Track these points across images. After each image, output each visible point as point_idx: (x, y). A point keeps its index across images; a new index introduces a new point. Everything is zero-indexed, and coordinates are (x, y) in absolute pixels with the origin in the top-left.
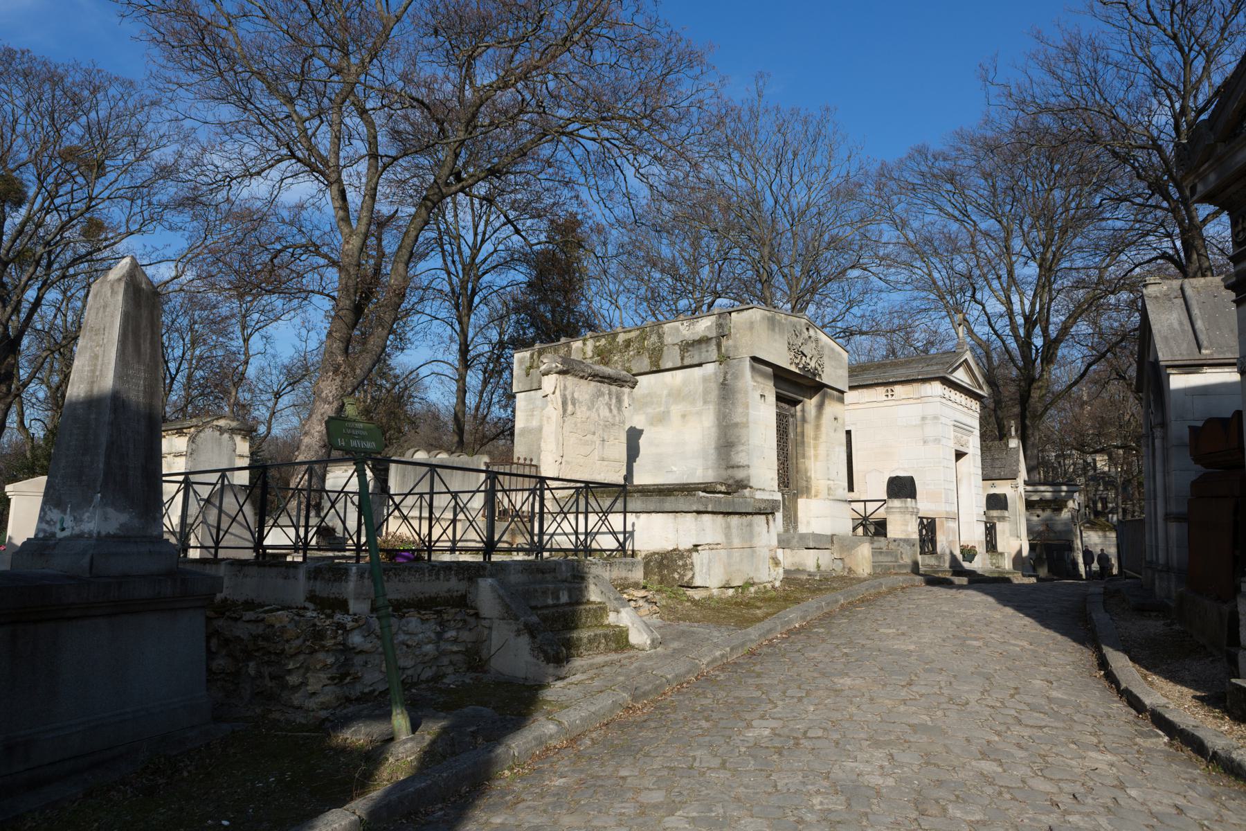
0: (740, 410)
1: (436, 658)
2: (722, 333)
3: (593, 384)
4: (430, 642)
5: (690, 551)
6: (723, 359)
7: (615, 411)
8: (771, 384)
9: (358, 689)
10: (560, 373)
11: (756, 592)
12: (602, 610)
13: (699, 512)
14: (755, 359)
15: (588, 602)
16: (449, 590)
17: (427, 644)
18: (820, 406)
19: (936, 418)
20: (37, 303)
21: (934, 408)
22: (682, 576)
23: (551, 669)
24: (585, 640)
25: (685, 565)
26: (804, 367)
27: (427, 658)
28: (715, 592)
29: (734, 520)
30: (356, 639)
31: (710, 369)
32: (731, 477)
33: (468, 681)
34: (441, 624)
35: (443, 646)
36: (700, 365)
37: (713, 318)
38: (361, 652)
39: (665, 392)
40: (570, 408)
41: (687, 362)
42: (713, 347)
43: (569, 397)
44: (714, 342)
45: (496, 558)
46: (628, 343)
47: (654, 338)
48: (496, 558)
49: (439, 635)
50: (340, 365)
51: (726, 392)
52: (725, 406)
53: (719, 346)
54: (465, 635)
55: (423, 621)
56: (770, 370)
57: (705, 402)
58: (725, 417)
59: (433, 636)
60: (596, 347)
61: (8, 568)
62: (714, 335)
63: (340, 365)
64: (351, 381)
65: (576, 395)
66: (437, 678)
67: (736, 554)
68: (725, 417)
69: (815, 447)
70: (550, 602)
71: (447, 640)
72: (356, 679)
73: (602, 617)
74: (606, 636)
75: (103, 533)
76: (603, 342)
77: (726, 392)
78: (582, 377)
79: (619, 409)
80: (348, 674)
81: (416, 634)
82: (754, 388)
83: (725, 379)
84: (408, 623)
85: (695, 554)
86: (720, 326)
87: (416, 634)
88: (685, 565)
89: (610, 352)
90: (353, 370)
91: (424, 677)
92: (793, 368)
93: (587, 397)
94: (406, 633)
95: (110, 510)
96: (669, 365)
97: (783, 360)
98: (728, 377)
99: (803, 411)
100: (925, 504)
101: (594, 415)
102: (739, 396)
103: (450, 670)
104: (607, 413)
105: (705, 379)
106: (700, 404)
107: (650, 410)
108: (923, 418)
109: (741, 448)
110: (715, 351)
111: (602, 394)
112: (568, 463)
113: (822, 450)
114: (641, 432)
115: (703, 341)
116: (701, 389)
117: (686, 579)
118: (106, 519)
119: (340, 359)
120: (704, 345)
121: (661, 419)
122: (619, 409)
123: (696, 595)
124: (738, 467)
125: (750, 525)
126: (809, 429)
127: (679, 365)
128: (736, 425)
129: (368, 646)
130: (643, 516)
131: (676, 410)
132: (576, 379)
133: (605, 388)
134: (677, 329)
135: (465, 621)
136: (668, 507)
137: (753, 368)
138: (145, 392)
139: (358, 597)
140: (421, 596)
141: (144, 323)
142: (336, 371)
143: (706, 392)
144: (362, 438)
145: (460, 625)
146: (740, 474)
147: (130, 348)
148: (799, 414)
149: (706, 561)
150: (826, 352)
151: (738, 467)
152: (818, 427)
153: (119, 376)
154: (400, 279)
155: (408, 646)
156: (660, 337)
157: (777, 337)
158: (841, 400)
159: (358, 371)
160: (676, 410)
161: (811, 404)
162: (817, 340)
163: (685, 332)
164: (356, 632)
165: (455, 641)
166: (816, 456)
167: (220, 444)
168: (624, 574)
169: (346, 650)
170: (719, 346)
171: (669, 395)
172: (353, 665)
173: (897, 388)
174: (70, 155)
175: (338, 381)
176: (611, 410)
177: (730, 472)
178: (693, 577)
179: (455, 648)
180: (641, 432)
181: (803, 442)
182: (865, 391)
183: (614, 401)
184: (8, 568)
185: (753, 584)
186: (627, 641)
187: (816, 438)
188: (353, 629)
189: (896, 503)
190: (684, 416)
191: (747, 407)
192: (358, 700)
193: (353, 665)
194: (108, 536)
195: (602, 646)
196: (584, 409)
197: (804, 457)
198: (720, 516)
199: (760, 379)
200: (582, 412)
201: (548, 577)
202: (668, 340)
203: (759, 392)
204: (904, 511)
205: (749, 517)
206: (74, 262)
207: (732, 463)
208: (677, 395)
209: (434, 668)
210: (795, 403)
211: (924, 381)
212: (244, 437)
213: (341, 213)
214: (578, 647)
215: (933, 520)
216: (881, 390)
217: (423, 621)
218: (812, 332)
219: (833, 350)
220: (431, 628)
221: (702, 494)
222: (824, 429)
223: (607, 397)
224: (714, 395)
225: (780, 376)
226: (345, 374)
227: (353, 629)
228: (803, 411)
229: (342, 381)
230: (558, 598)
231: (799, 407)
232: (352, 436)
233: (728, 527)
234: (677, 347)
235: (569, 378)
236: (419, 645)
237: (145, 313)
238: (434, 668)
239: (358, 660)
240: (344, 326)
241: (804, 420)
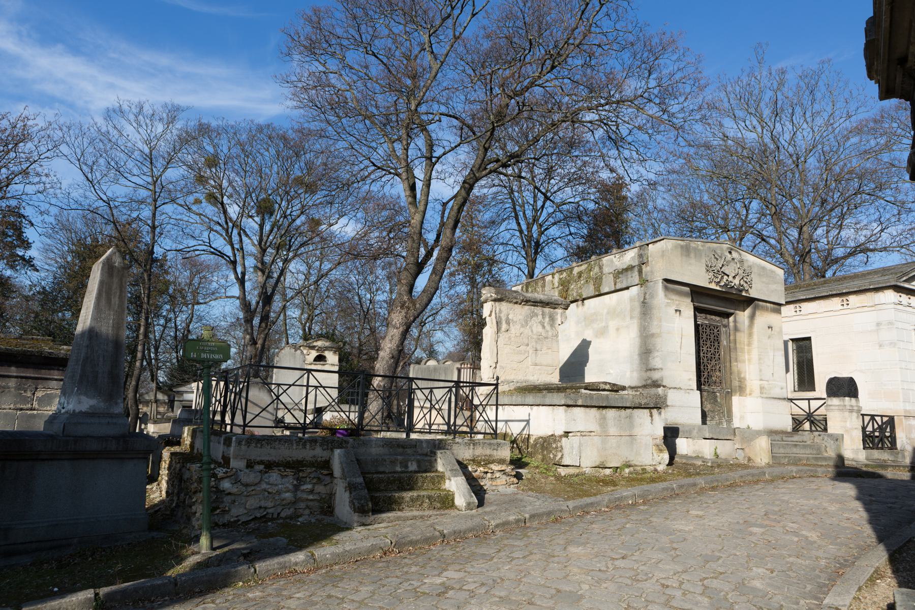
0: (655, 323)
1: (294, 503)
2: (643, 262)
3: (527, 307)
4: (288, 492)
5: (561, 437)
6: (643, 282)
7: (548, 327)
8: (689, 300)
9: (227, 518)
10: (495, 300)
11: (630, 473)
12: (442, 477)
13: (568, 406)
14: (667, 281)
15: (437, 471)
16: (314, 456)
17: (286, 492)
18: (752, 317)
19: (890, 323)
20: (282, 272)
21: (889, 314)
22: (555, 456)
23: (356, 517)
24: (407, 499)
25: (557, 448)
26: (726, 285)
27: (284, 502)
28: (588, 471)
29: (611, 413)
30: (226, 485)
31: (634, 290)
32: (650, 378)
33: (313, 520)
34: (298, 479)
35: (299, 494)
36: (627, 288)
37: (636, 250)
38: (229, 494)
39: (605, 311)
40: (504, 326)
41: (619, 286)
42: (636, 273)
43: (504, 319)
44: (636, 269)
45: (413, 436)
46: (580, 274)
47: (596, 269)
48: (413, 436)
49: (296, 488)
50: (405, 302)
51: (646, 308)
52: (645, 320)
53: (640, 272)
54: (320, 488)
55: (283, 477)
56: (687, 289)
57: (632, 318)
58: (645, 329)
59: (291, 487)
60: (560, 279)
61: (42, 429)
62: (637, 263)
63: (405, 302)
64: (412, 312)
65: (510, 317)
66: (296, 516)
67: (613, 441)
68: (645, 329)
69: (749, 352)
70: (398, 469)
71: (303, 491)
72: (224, 512)
73: (439, 483)
74: (429, 497)
75: (77, 411)
76: (565, 275)
77: (646, 308)
78: (516, 303)
79: (552, 326)
80: (219, 508)
81: (276, 485)
82: (668, 305)
83: (645, 299)
84: (269, 477)
85: (564, 439)
86: (640, 256)
87: (276, 485)
88: (557, 448)
89: (569, 282)
90: (414, 305)
91: (283, 515)
92: (713, 286)
93: (521, 317)
94: (268, 483)
95: (83, 398)
96: (606, 290)
97: (702, 279)
98: (647, 297)
99: (735, 321)
100: (871, 401)
101: (527, 331)
102: (655, 312)
103: (307, 512)
104: (540, 329)
105: (632, 300)
106: (628, 319)
107: (595, 326)
108: (878, 324)
109: (656, 354)
110: (637, 277)
111: (537, 315)
112: (502, 367)
113: (755, 353)
114: (590, 343)
115: (630, 268)
116: (629, 308)
117: (557, 458)
118: (80, 402)
119: (405, 298)
120: (629, 272)
121: (602, 332)
122: (552, 326)
123: (563, 471)
124: (655, 369)
125: (630, 417)
126: (742, 337)
127: (613, 289)
128: (653, 335)
129: (234, 490)
130: (535, 408)
131: (613, 324)
132: (511, 305)
133: (538, 310)
134: (612, 261)
135: (319, 478)
136: (548, 402)
137: (666, 289)
138: (113, 327)
139: (236, 457)
140: (288, 459)
141: (115, 286)
142: (402, 307)
143: (632, 310)
144: (213, 352)
145: (315, 481)
146: (656, 376)
147: (103, 302)
148: (731, 324)
149: (576, 445)
150: (755, 270)
151: (655, 369)
152: (750, 335)
153: (94, 318)
154: (448, 240)
155: (269, 493)
156: (601, 268)
157: (693, 261)
158: (779, 312)
159: (418, 306)
160: (613, 324)
161: (743, 316)
162: (742, 261)
163: (617, 263)
164: (226, 480)
165: (311, 492)
166: (749, 360)
167: (295, 357)
168: (488, 452)
169: (219, 492)
170: (640, 272)
171: (608, 313)
172: (223, 502)
173: (852, 298)
174: (299, 181)
175: (403, 313)
176: (544, 327)
177: (648, 373)
178: (562, 457)
179: (311, 497)
180: (590, 343)
181: (736, 349)
182: (822, 302)
183: (547, 319)
184: (42, 429)
185: (630, 466)
186: (453, 502)
187: (749, 344)
188: (223, 478)
189: (835, 401)
190: (618, 329)
191: (660, 321)
192: (224, 525)
193: (223, 502)
194: (81, 412)
195: (425, 505)
196: (518, 326)
197: (736, 361)
198: (594, 410)
199: (674, 297)
200: (515, 329)
201: (409, 451)
202: (606, 270)
203: (675, 307)
204: (842, 409)
205: (628, 411)
206: (302, 245)
207: (650, 366)
208: (613, 313)
209: (292, 510)
210: (728, 315)
211: (877, 290)
212: (335, 352)
213: (410, 199)
214: (400, 504)
215: (891, 420)
216: (837, 300)
217: (283, 477)
218: (735, 255)
219: (764, 268)
220: (289, 482)
221: (583, 391)
222: (755, 337)
223: (540, 317)
224: (637, 310)
225: (696, 292)
226: (408, 308)
227: (223, 478)
228: (735, 321)
229: (407, 313)
230: (407, 467)
231: (731, 319)
232: (204, 351)
233: (604, 418)
234: (611, 275)
235: (504, 304)
236: (279, 492)
237: (116, 280)
238: (292, 510)
239: (228, 499)
240: (409, 275)
241: (736, 329)
